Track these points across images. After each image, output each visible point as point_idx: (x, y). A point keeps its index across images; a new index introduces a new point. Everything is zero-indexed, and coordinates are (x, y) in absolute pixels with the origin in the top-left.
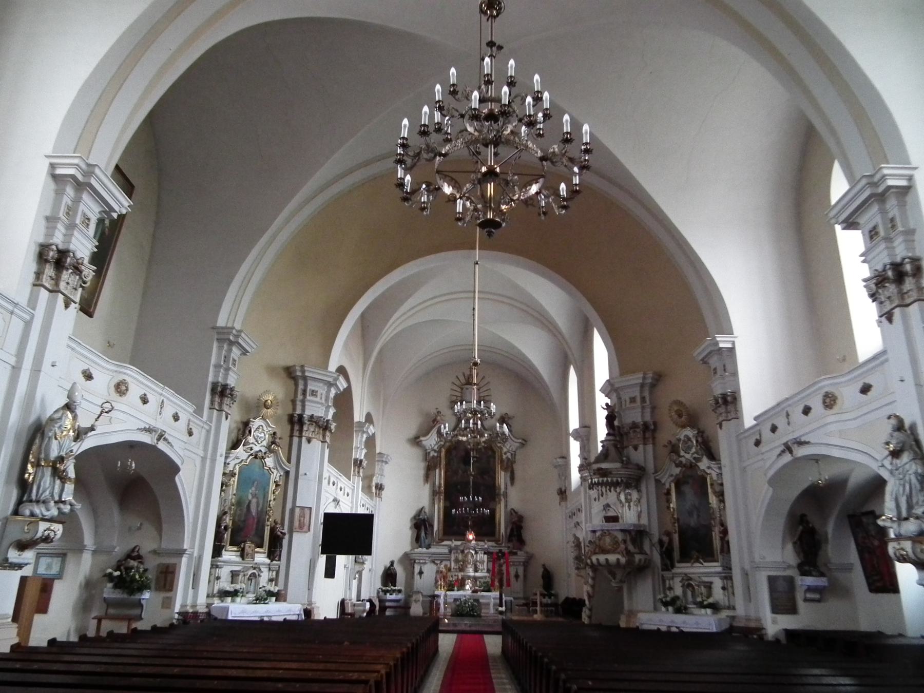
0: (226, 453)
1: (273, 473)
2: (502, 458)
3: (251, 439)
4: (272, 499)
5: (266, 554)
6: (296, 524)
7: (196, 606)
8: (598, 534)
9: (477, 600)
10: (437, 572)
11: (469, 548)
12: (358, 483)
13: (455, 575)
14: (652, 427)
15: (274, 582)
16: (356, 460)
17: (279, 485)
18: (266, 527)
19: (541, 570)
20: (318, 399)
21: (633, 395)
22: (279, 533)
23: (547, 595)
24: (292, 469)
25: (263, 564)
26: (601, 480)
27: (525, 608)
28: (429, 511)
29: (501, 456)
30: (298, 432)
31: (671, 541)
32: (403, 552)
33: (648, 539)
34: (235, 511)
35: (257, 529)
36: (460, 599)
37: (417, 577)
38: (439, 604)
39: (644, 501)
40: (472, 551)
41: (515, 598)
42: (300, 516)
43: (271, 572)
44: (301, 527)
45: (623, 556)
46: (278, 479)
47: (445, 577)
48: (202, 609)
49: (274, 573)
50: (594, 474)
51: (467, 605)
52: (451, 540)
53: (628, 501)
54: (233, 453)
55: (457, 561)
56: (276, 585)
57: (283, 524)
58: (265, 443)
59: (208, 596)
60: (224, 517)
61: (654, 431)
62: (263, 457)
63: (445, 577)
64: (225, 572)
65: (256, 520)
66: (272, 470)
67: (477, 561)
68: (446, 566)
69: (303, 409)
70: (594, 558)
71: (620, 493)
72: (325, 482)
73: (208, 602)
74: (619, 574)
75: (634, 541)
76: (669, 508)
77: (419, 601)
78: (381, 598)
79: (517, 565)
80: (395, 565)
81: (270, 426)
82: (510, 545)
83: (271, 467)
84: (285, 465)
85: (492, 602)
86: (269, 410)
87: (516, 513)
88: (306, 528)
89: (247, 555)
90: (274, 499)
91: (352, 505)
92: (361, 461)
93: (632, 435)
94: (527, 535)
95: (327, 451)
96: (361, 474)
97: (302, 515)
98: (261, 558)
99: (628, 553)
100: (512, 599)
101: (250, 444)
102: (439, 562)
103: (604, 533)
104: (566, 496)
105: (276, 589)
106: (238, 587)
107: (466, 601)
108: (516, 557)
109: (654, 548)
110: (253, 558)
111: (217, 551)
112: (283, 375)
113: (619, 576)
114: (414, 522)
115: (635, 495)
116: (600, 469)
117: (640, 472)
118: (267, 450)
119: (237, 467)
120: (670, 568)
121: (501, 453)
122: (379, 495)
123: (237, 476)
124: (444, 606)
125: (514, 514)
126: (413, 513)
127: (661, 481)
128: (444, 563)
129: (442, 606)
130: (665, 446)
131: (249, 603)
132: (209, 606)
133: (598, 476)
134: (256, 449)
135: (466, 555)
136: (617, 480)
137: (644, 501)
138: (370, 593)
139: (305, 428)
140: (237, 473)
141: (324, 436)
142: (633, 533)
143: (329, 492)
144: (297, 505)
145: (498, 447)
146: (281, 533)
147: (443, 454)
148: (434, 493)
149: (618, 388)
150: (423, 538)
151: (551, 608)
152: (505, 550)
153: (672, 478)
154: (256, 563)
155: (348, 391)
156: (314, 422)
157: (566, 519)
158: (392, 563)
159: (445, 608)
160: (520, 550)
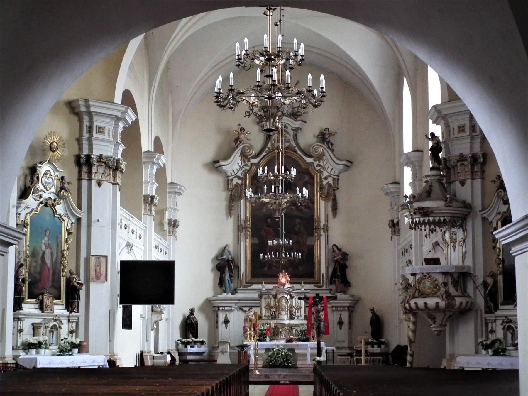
0: (17, 203)
1: (64, 221)
2: (321, 184)
3: (40, 186)
4: (66, 248)
5: (64, 306)
6: (93, 273)
7: (5, 358)
8: (418, 277)
9: (292, 350)
10: (246, 320)
11: (283, 293)
12: (150, 222)
14: (481, 160)
15: (74, 334)
16: (146, 197)
17: (71, 233)
18: (62, 278)
19: (370, 315)
20: (106, 137)
21: (461, 123)
22: (76, 284)
23: (376, 344)
24: (83, 215)
25: (63, 316)
26: (422, 219)
27: (349, 357)
29: (321, 182)
30: (87, 174)
31: (495, 283)
32: (206, 298)
33: (472, 282)
34: (31, 263)
35: (53, 280)
36: (273, 349)
37: (221, 326)
38: (249, 356)
39: (469, 240)
40: (286, 296)
41: (337, 348)
42: (96, 266)
43: (70, 324)
44: (98, 277)
45: (443, 300)
46: (69, 227)
47: (255, 326)
48: (10, 360)
49: (74, 324)
50: (415, 213)
51: (280, 355)
52: (261, 283)
53: (453, 241)
54: (24, 203)
55: (268, 307)
56: (77, 337)
57: (78, 274)
58: (53, 189)
59: (13, 349)
60: (21, 269)
61: (484, 163)
62: (53, 204)
63: (255, 326)
64: (26, 325)
65: (51, 272)
66: (63, 217)
67: (292, 307)
68: (255, 313)
69: (91, 149)
70: (412, 302)
71: (445, 233)
72: (118, 227)
73: (14, 355)
74: (439, 318)
75: (456, 284)
76: (494, 247)
77: (226, 352)
78: (180, 351)
79: (340, 310)
80: (196, 314)
81: (57, 170)
82: (333, 287)
83: (62, 215)
84: (76, 212)
85: (309, 352)
86: (55, 153)
87: (339, 250)
88: (103, 278)
89: (46, 308)
90: (68, 249)
91: (145, 248)
92: (153, 197)
93: (459, 169)
94: (351, 276)
95: (119, 193)
96: (153, 213)
97: (98, 265)
98: (60, 310)
99: (448, 296)
100: (334, 349)
101: (39, 191)
102: (247, 309)
103: (426, 276)
104: (399, 230)
105: (77, 341)
106: (41, 339)
108: (335, 301)
109: (478, 293)
110: (52, 310)
111: (18, 304)
112: (67, 110)
113: (439, 320)
114: (218, 262)
115: (460, 234)
116: (420, 209)
117: (465, 210)
118: (56, 197)
119: (28, 217)
120: (493, 311)
121: (321, 178)
122: (172, 233)
123: (29, 227)
124: (255, 357)
125: (337, 251)
126: (214, 252)
127: (488, 220)
128: (254, 310)
129: (252, 358)
130: (494, 181)
131: (53, 355)
132: (15, 358)
133: (420, 216)
134: (46, 196)
135: (279, 300)
136: (440, 220)
137: (469, 240)
138: (168, 346)
139: (94, 170)
140: (29, 223)
141: (115, 178)
142: (456, 276)
143: (122, 236)
144: (92, 254)
145: (317, 171)
146: (78, 283)
148: (240, 228)
149: (446, 115)
150: (227, 282)
151: (378, 357)
152: (324, 294)
153: (499, 216)
154: (57, 316)
155: (136, 123)
156: (103, 162)
157: (398, 257)
158: (192, 311)
159: (256, 359)
160: (345, 292)
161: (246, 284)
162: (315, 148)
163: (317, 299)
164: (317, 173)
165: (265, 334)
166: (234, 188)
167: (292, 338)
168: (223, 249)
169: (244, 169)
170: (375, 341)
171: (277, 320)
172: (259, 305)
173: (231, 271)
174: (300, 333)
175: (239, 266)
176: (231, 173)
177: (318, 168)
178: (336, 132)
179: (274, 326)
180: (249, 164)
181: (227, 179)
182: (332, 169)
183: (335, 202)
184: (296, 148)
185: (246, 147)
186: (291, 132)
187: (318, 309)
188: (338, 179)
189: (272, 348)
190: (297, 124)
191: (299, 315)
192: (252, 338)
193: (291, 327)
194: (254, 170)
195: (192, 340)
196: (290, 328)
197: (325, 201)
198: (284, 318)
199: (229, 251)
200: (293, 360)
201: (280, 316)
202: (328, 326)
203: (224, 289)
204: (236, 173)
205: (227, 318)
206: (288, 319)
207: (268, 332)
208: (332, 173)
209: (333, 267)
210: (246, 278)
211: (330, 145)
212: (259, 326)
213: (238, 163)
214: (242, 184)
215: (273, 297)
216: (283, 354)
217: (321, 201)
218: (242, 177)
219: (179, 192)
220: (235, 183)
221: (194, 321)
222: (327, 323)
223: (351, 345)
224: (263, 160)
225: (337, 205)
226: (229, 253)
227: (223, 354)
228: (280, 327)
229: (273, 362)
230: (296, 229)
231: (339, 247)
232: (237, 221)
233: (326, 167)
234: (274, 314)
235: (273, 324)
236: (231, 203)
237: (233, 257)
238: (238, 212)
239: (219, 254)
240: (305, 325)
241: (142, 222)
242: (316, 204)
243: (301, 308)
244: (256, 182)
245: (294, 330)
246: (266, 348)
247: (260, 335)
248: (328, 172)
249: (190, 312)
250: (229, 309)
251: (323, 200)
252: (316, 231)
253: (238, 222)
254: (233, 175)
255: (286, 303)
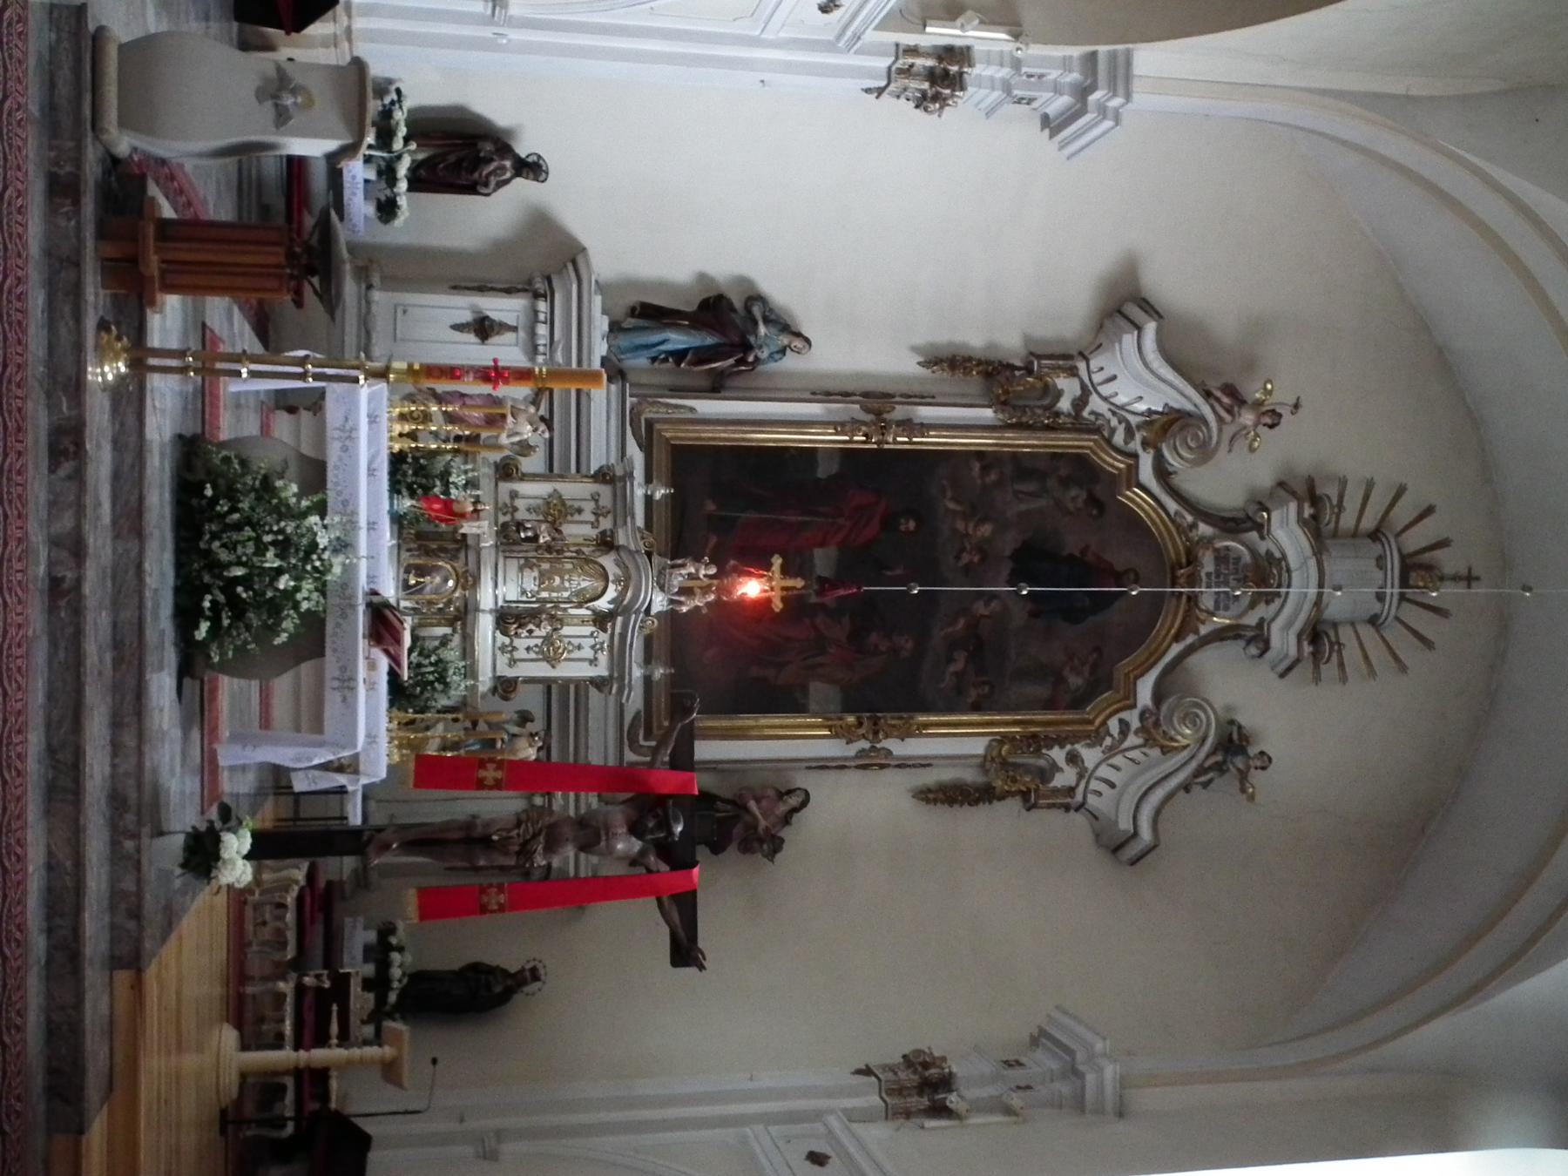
2: (1051, 742)
11: (625, 581)
13: (477, 501)
19: (512, 962)
23: (381, 1000)
28: (790, 375)
40: (611, 592)
51: (271, 560)
55: (556, 511)
67: (557, 621)
68: (525, 448)
77: (282, 118)
87: (786, 820)
107: (297, 550)
114: (738, 303)
121: (1075, 738)
125: (782, 808)
126: (778, 293)
135: (588, 561)
145: (1104, 723)
147: (1066, 442)
158: (532, 168)
161: (646, 420)
162: (1197, 716)
163: (679, 829)
164: (1097, 722)
165: (427, 489)
166: (1040, 378)
167: (398, 641)
168: (793, 329)
169: (1114, 422)
170: (393, 997)
171: (493, 551)
172: (556, 470)
173: (702, 356)
174: (433, 659)
175: (722, 394)
176: (1102, 369)
177: (1113, 724)
178: (1252, 798)
179: (464, 535)
180: (1136, 445)
181: (1074, 353)
182: (1112, 785)
183: (980, 795)
184: (1190, 639)
185: (1204, 428)
186: (1251, 619)
187: (610, 835)
188: (1067, 808)
189: (330, 505)
190: (1284, 640)
191: (517, 655)
192: (407, 428)
193: (463, 616)
194: (1113, 466)
195: (399, 157)
196: (457, 609)
197: (985, 757)
198: (505, 584)
199: (783, 351)
200: (241, 650)
201: (513, 565)
202: (483, 910)
203: (625, 325)
204: (1099, 388)
205: (498, 333)
206: (500, 603)
207: (436, 506)
208: (1094, 785)
209: (715, 791)
210: (665, 421)
211: (1203, 775)
212: (466, 463)
213: (1141, 398)
214: (1058, 414)
215: (603, 533)
216: (284, 582)
217: (985, 741)
218: (1085, 414)
219: (1090, 108)
220: (1059, 387)
221: (490, 174)
222: (502, 898)
223: (374, 876)
224: (1149, 505)
225: (966, 806)
226: (778, 352)
227: (261, 95)
228: (459, 565)
229: (223, 506)
230: (874, 637)
231: (796, 817)
232: (905, 389)
233: (1118, 760)
234: (523, 535)
235: (475, 531)
236: (981, 368)
237: (760, 368)
238: (944, 395)
239: (771, 310)
240: (470, 682)
241: (876, 29)
242: (975, 718)
243: (552, 661)
244: (1064, 472)
245: (448, 630)
246: (332, 461)
247: (423, 467)
248: (1097, 767)
249: (530, 160)
250: (541, 341)
251: (989, 747)
252: (865, 721)
253: (901, 396)
254: (1090, 379)
255: (578, 593)
